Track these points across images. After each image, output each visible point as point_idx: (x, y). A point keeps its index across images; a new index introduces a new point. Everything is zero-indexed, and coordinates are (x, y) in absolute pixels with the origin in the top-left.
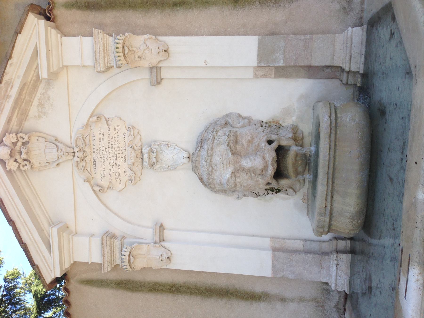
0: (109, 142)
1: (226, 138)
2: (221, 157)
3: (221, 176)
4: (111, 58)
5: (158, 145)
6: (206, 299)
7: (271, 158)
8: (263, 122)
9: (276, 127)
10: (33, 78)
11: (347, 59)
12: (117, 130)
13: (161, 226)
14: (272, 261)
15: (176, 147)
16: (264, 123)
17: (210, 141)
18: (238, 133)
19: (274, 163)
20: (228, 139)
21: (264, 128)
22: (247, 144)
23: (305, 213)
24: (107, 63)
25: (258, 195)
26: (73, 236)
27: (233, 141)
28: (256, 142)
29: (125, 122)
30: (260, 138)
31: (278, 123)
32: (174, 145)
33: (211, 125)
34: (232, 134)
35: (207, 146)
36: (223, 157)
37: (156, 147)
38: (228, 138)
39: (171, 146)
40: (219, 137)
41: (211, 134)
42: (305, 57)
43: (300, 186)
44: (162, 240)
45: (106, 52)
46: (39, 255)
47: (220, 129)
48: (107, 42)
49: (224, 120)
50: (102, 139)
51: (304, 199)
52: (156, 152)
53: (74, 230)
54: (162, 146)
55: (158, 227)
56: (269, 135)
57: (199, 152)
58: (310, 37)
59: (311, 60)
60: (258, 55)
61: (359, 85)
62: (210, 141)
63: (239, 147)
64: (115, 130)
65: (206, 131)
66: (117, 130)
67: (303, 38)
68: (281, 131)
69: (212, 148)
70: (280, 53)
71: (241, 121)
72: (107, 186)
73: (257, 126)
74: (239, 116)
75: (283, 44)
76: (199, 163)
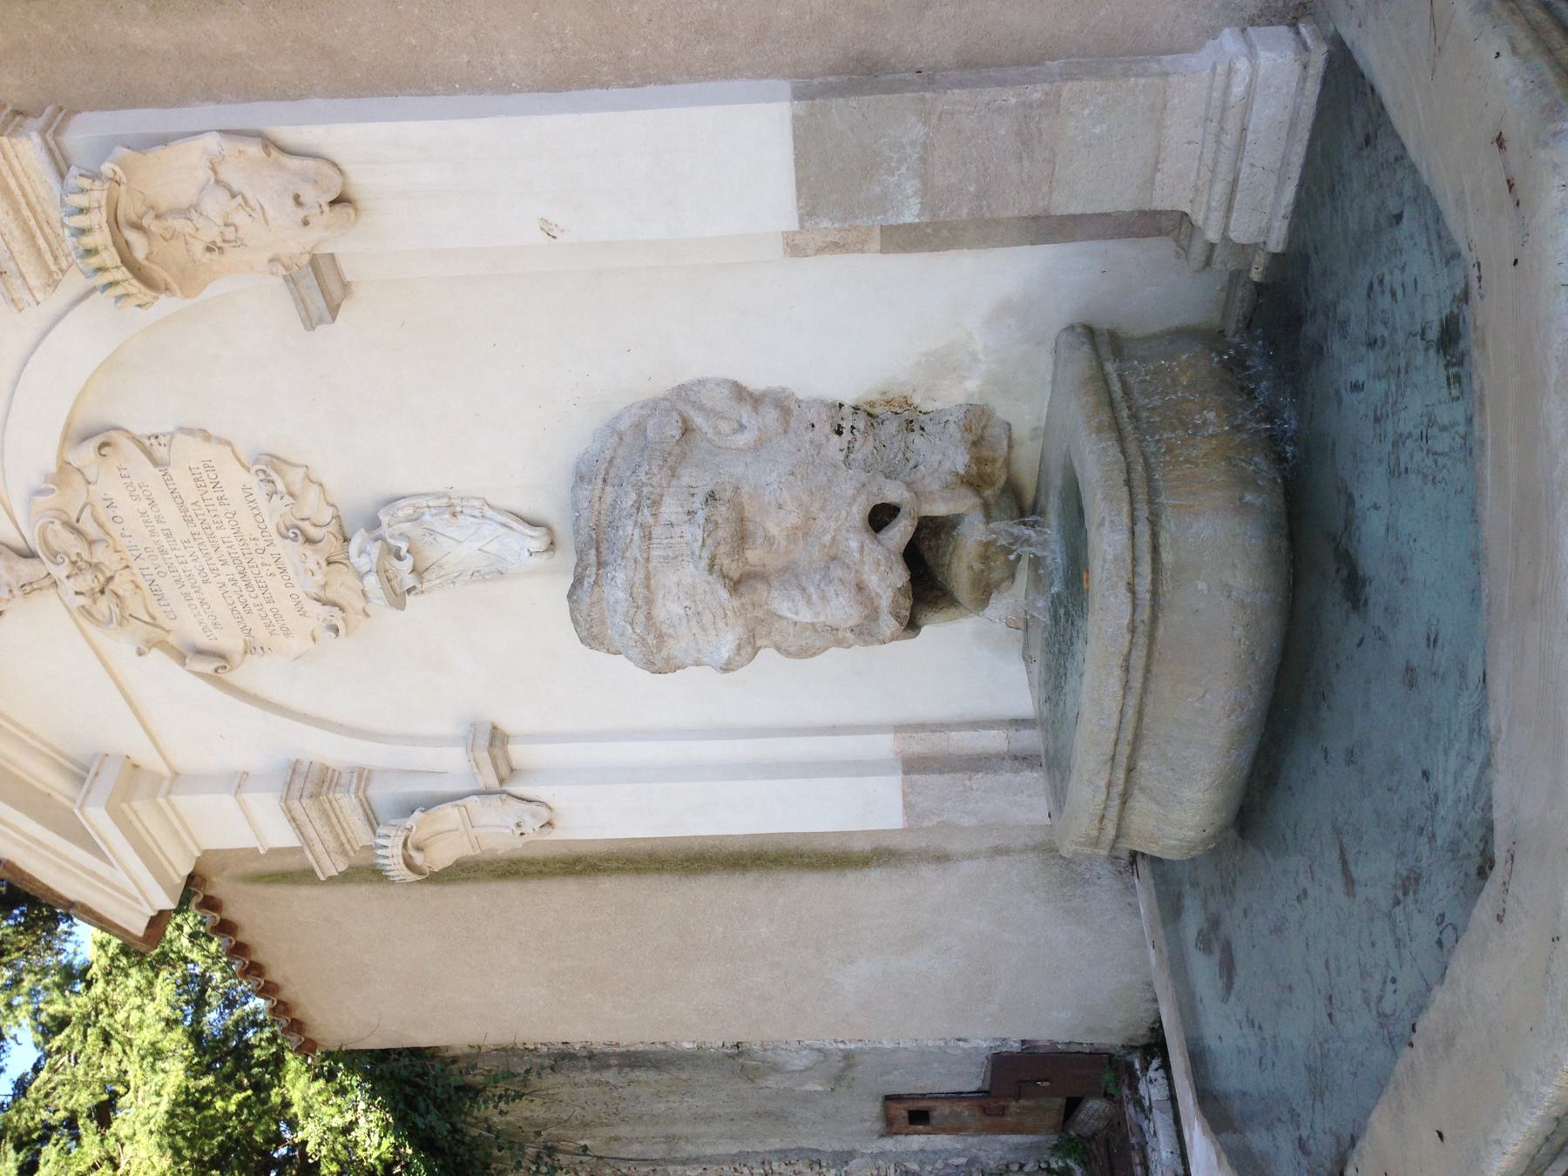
0: (189, 521)
2: (687, 603)
5: (413, 519)
6: (691, 877)
8: (841, 405)
11: (1216, 197)
12: (207, 481)
13: (497, 738)
14: (905, 795)
15: (489, 512)
17: (634, 552)
18: (746, 496)
20: (709, 541)
21: (850, 437)
23: (1016, 653)
24: (56, 258)
26: (169, 792)
28: (825, 531)
29: (228, 443)
31: (906, 402)
32: (477, 503)
36: (695, 601)
37: (406, 527)
39: (466, 511)
42: (1022, 181)
45: (30, 214)
47: (664, 483)
48: (18, 168)
50: (151, 514)
52: (408, 551)
53: (165, 771)
54: (427, 517)
55: (484, 741)
57: (596, 589)
58: (1047, 94)
59: (1051, 194)
60: (800, 184)
61: (1255, 275)
62: (634, 552)
63: (754, 555)
64: (197, 480)
65: (604, 481)
66: (207, 481)
67: (1013, 101)
69: (648, 578)
70: (903, 170)
72: (240, 646)
74: (740, 392)
75: (918, 131)
76: (603, 622)
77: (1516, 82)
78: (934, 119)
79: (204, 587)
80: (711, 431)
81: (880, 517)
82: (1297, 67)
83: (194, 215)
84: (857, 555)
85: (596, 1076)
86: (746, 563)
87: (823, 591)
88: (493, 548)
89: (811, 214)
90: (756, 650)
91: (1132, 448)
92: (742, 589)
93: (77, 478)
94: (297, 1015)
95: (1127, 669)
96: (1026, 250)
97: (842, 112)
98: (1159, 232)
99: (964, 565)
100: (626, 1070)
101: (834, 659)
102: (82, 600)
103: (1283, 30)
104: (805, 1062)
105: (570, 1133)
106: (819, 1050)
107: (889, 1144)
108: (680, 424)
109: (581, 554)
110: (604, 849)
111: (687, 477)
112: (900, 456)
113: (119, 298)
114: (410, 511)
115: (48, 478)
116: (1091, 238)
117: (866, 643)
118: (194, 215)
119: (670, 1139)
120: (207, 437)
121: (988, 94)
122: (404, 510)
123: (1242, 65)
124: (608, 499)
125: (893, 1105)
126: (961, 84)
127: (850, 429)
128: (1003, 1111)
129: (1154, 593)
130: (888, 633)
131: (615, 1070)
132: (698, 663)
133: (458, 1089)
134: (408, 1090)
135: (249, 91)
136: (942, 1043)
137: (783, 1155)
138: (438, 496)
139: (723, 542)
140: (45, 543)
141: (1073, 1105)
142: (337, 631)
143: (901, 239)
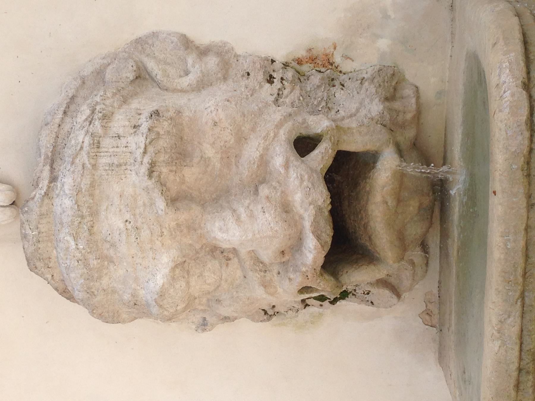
1: (143, 146)
2: (128, 216)
3: (136, 279)
7: (312, 207)
8: (273, 61)
9: (323, 79)
16: (278, 65)
17: (84, 158)
19: (322, 223)
20: (151, 149)
21: (279, 86)
22: (222, 158)
23: (432, 357)
25: (270, 312)
27: (167, 157)
30: (268, 134)
33: (84, 83)
34: (164, 126)
35: (74, 180)
38: (150, 143)
40: (113, 142)
41: (83, 132)
43: (414, 274)
47: (115, 105)
49: (131, 63)
51: (429, 313)
56: (300, 119)
57: (46, 201)
62: (84, 158)
65: (65, 113)
68: (339, 94)
69: (92, 185)
71: (193, 66)
73: (252, 82)
80: (160, 73)
84: (282, 171)
87: (251, 210)
108: (135, 68)
112: (323, 104)
127: (280, 80)
139: (163, 151)
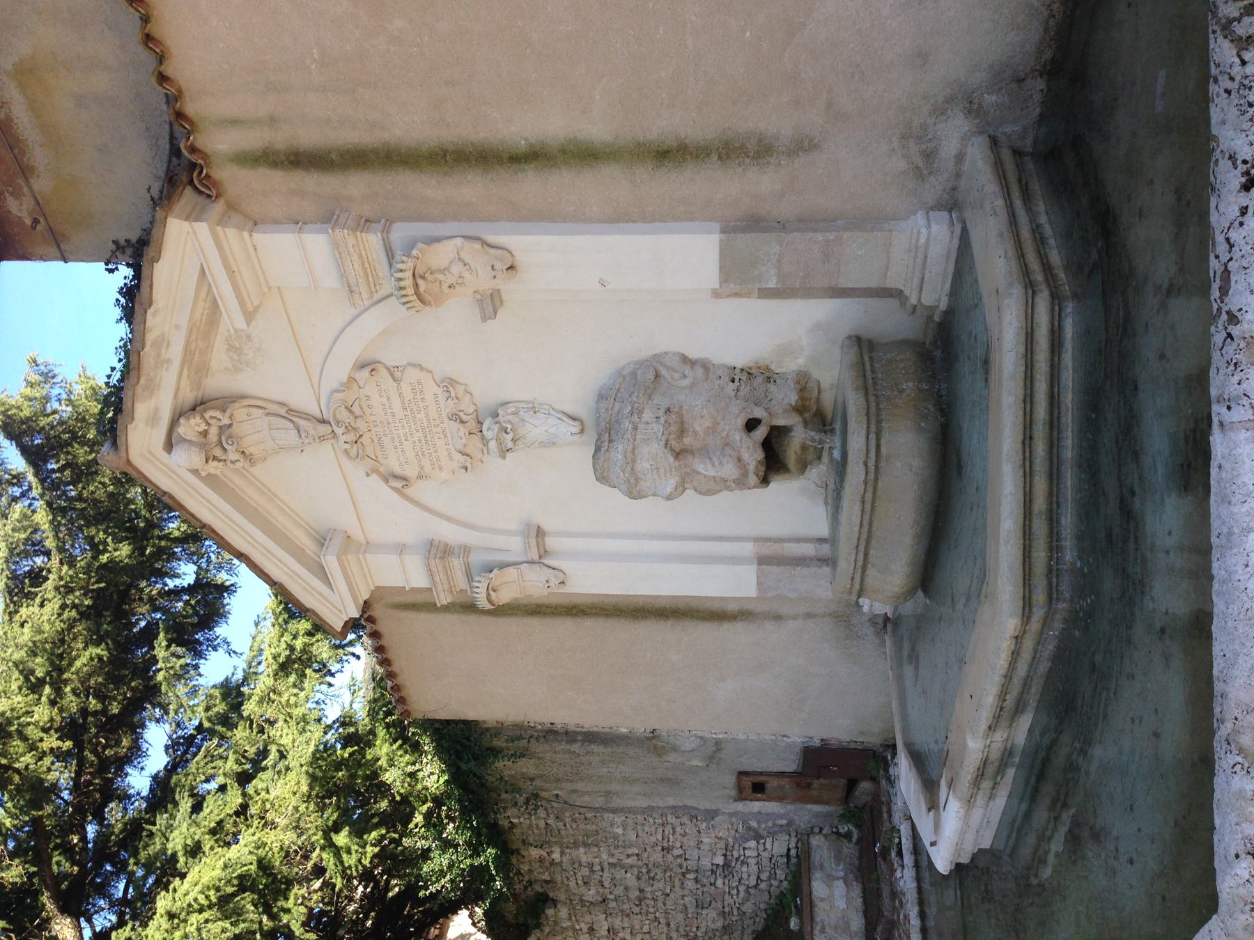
0: (405, 409)
4: (380, 274)
5: (515, 413)
10: (206, 312)
13: (540, 533)
15: (552, 412)
17: (628, 435)
26: (365, 552)
29: (431, 372)
31: (768, 368)
32: (546, 407)
37: (510, 417)
44: (544, 552)
46: (312, 594)
53: (363, 541)
54: (521, 413)
55: (534, 534)
62: (628, 435)
63: (687, 440)
69: (634, 449)
74: (685, 359)
75: (777, 249)
77: (1003, 270)
78: (784, 244)
79: (404, 443)
81: (752, 425)
82: (949, 234)
83: (447, 273)
85: (568, 747)
86: (683, 444)
88: (553, 430)
89: (726, 281)
90: (685, 489)
91: (872, 399)
92: (680, 457)
93: (355, 386)
94: (403, 694)
95: (863, 502)
96: (829, 301)
97: (743, 240)
98: (891, 296)
99: (792, 451)
100: (587, 744)
101: (725, 499)
102: (347, 446)
103: (945, 214)
104: (693, 746)
105: (548, 785)
106: (701, 738)
107: (740, 807)
109: (600, 435)
110: (589, 601)
111: (657, 400)
113: (408, 309)
114: (514, 409)
115: (342, 384)
116: (859, 297)
117: (741, 489)
118: (447, 273)
119: (608, 794)
120: (422, 369)
121: (810, 235)
122: (511, 409)
123: (924, 231)
124: (616, 408)
125: (745, 778)
126: (798, 230)
128: (809, 786)
129: (877, 467)
130: (752, 483)
131: (579, 744)
132: (654, 495)
133: (488, 749)
134: (459, 747)
135: (474, 217)
136: (774, 738)
137: (675, 810)
138: (528, 402)
140: (334, 416)
141: (852, 784)
142: (466, 469)
143: (766, 294)
